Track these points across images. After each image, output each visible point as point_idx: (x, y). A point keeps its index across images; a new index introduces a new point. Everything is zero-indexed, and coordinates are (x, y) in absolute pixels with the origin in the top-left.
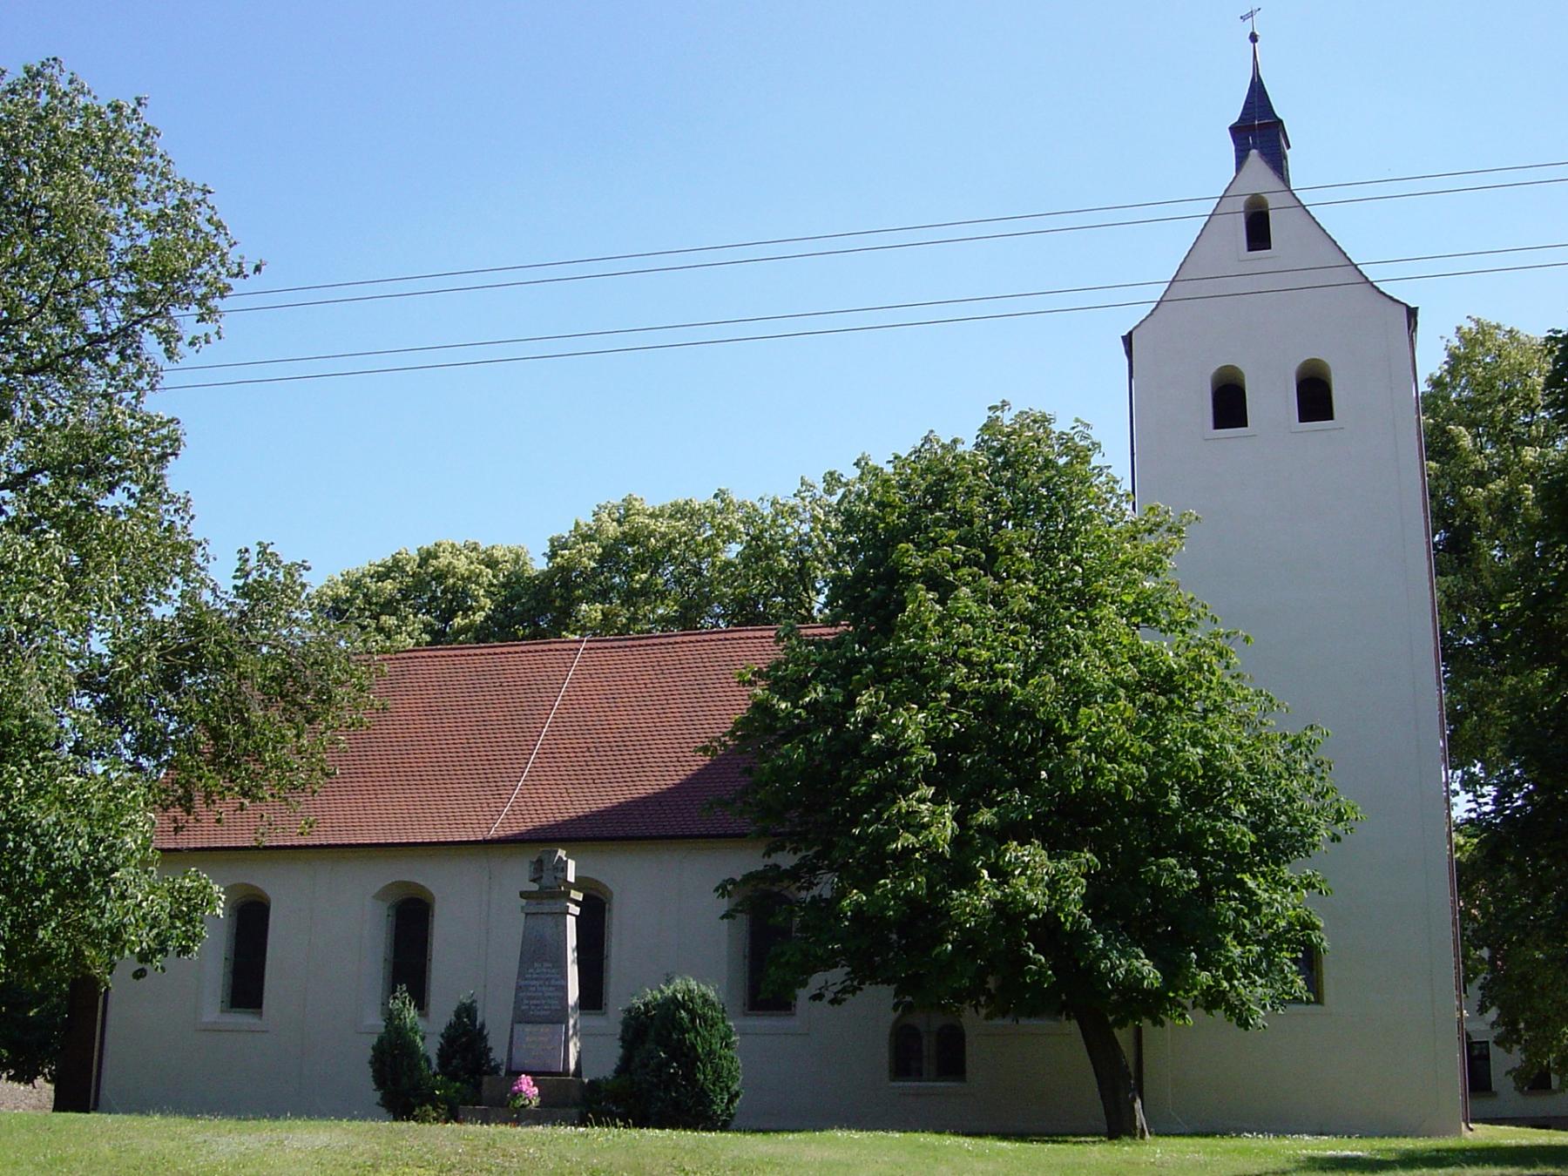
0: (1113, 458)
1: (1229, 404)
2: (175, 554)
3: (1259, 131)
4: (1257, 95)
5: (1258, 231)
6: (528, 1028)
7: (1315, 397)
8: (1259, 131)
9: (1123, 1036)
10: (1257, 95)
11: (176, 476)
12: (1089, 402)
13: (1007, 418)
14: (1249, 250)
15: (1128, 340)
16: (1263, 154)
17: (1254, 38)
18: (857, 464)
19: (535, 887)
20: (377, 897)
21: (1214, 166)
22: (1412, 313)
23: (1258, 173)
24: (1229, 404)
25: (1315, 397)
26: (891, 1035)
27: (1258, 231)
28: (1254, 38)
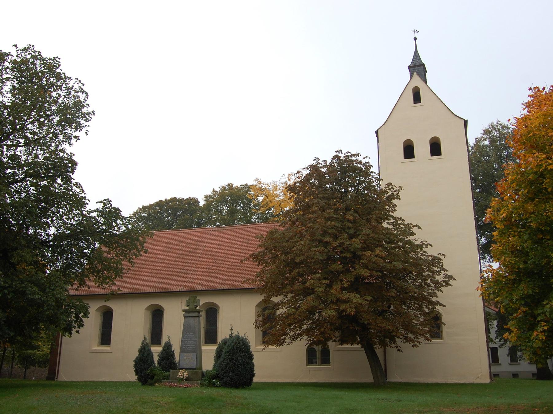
0: (375, 169)
1: (409, 151)
2: (79, 202)
3: (417, 68)
4: (416, 55)
5: (417, 98)
6: (185, 354)
7: (435, 148)
8: (417, 68)
9: (379, 351)
10: (416, 55)
11: (77, 177)
12: (367, 152)
13: (342, 156)
14: (415, 103)
15: (377, 132)
16: (418, 74)
17: (415, 39)
18: (93, 112)
19: (187, 308)
20: (147, 309)
21: (403, 77)
22: (466, 122)
23: (417, 82)
24: (409, 151)
25: (435, 148)
26: (307, 350)
27: (417, 98)
28: (415, 39)
